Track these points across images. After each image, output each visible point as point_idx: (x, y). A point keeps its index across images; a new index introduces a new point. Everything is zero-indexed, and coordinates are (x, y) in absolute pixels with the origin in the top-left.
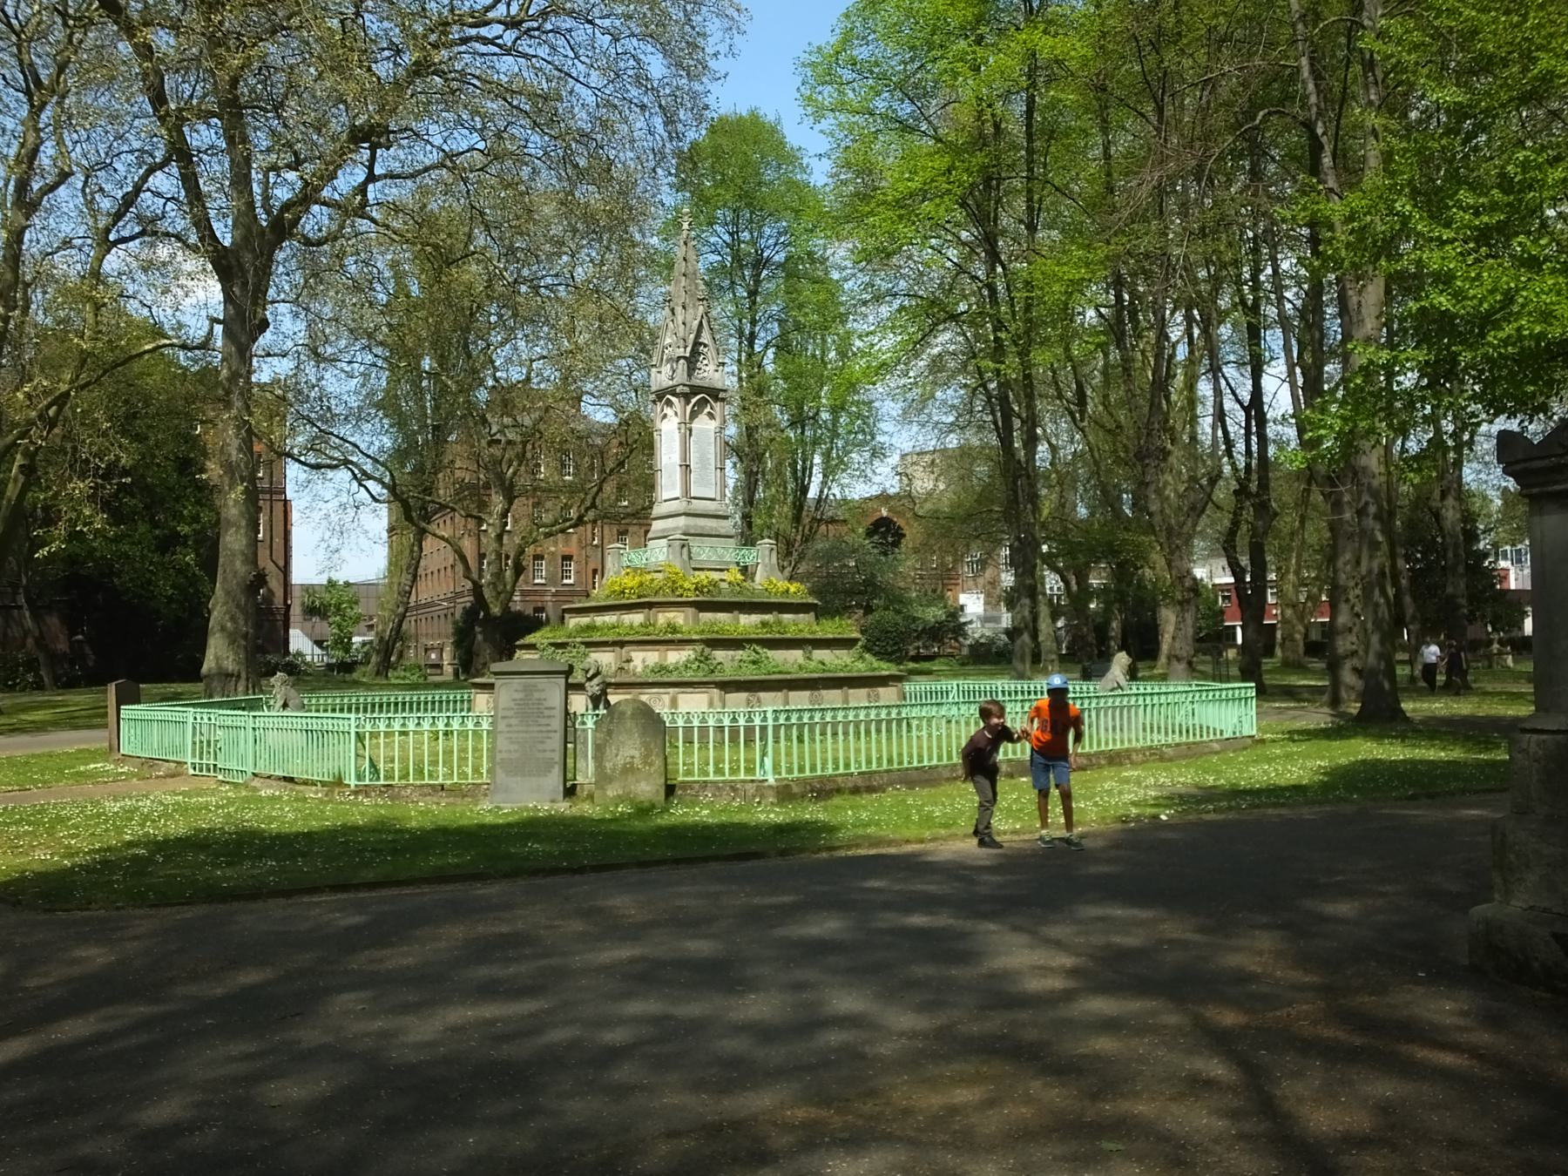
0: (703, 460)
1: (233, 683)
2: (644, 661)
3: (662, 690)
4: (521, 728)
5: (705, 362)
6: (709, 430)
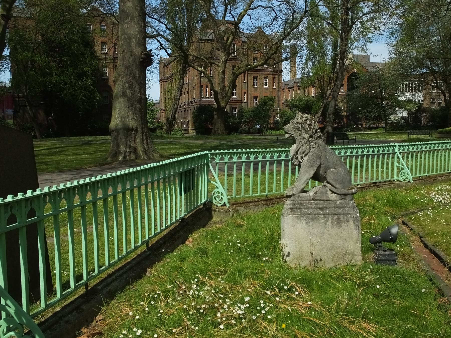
1: (133, 135)
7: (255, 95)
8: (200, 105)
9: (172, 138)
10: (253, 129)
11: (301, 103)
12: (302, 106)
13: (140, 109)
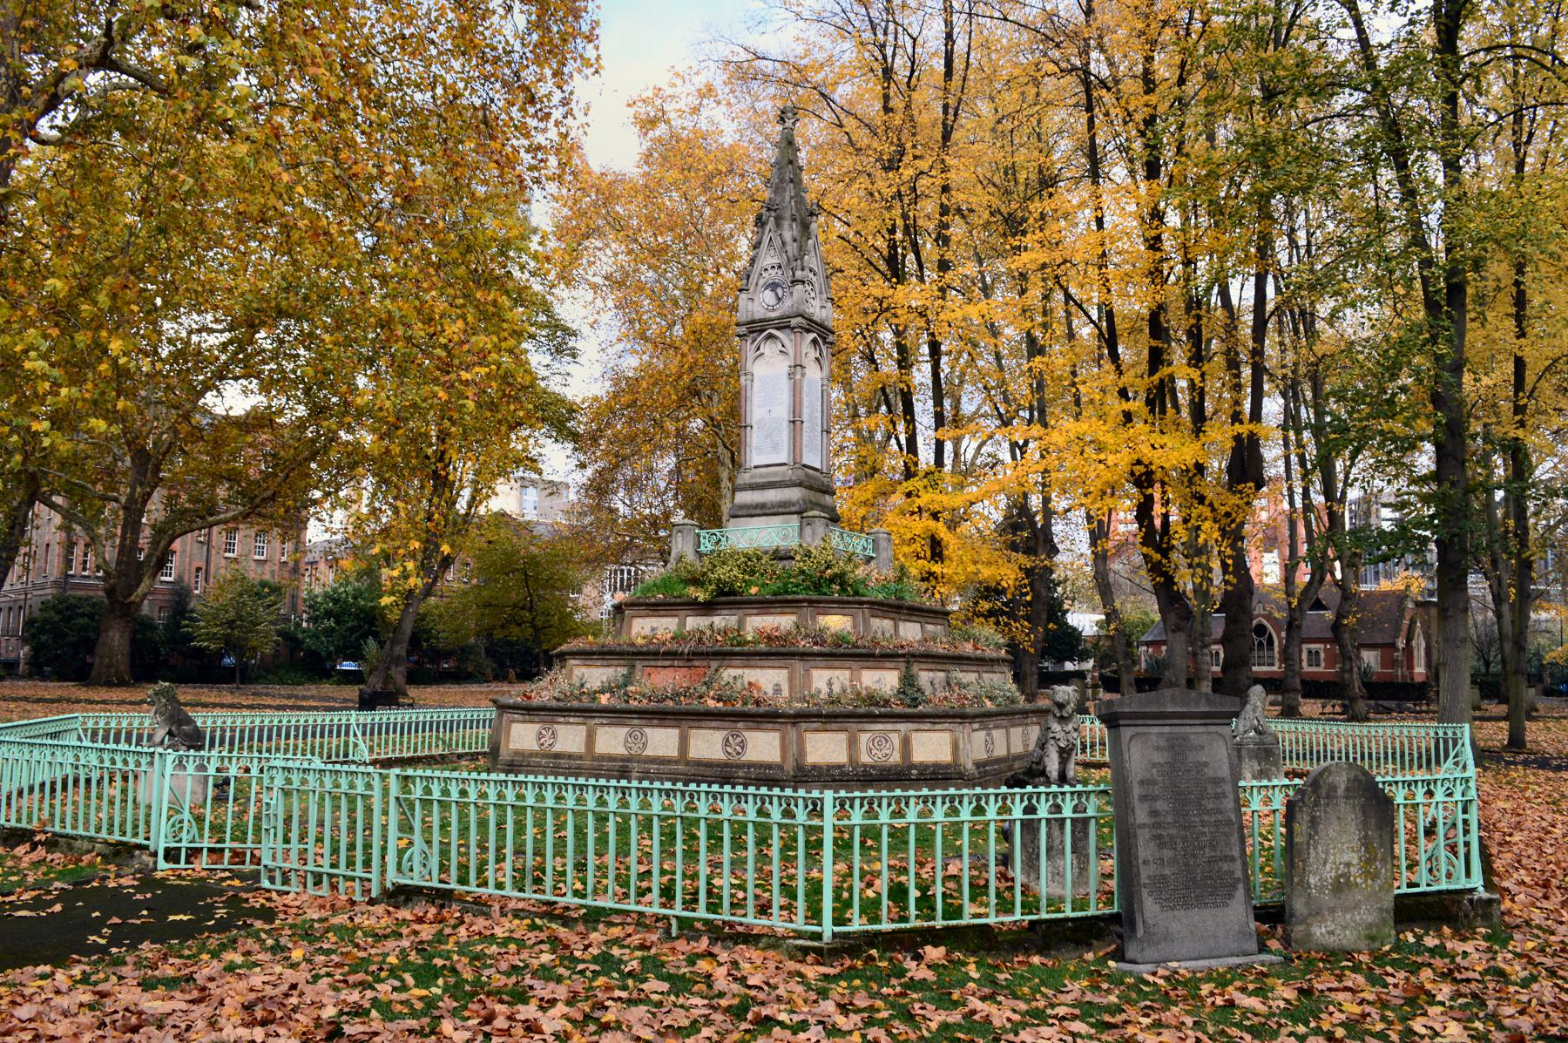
3: (889, 726)
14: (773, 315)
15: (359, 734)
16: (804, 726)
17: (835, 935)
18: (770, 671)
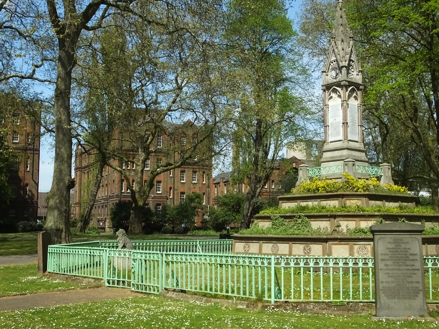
0: (353, 121)
2: (347, 226)
3: (367, 243)
4: (394, 267)
5: (353, 70)
6: (354, 105)
7: (182, 191)
8: (120, 201)
9: (86, 236)
10: (178, 229)
11: (231, 200)
12: (233, 204)
13: (65, 217)
14: (335, 80)
15: (201, 249)
16: (331, 243)
17: (275, 302)
18: (324, 222)
